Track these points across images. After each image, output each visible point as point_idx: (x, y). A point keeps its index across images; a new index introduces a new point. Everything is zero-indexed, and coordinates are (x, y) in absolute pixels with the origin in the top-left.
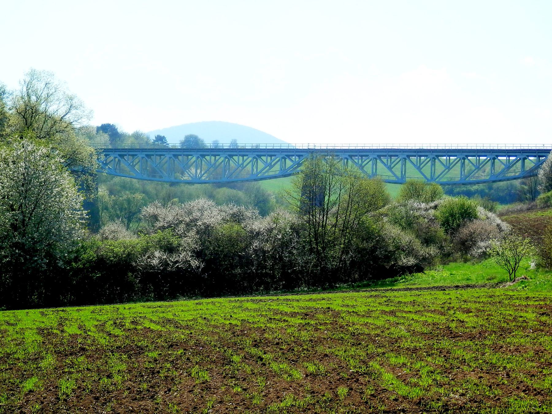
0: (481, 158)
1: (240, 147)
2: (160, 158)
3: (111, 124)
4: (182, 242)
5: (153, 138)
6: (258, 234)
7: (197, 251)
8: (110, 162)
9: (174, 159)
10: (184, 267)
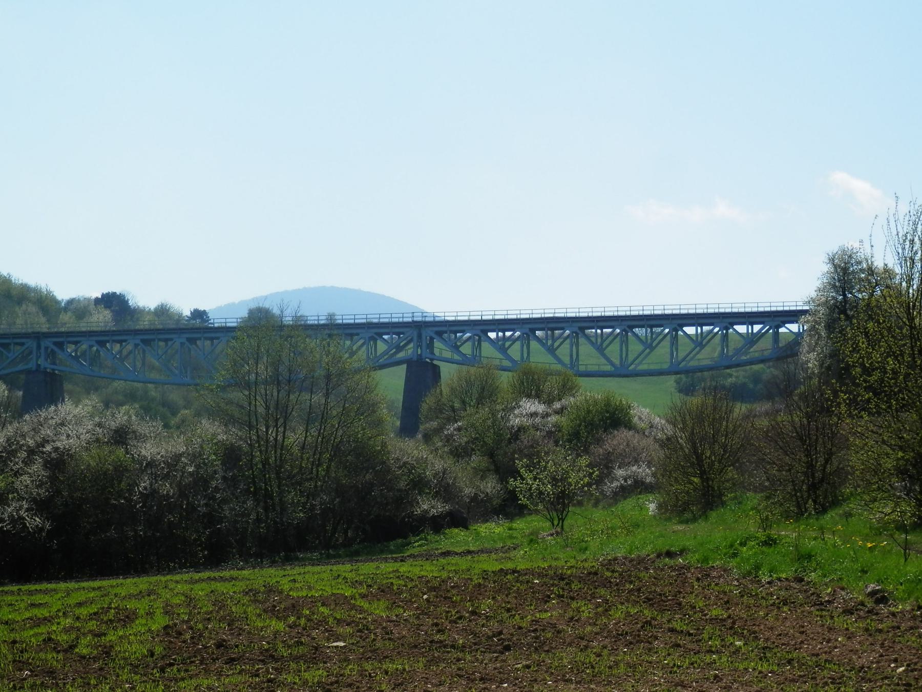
0: (604, 330)
1: (216, 325)
2: (212, 344)
3: (118, 293)
4: (17, 484)
5: (187, 313)
6: (150, 464)
7: (41, 499)
8: (127, 356)
9: (190, 347)
10: (13, 530)
